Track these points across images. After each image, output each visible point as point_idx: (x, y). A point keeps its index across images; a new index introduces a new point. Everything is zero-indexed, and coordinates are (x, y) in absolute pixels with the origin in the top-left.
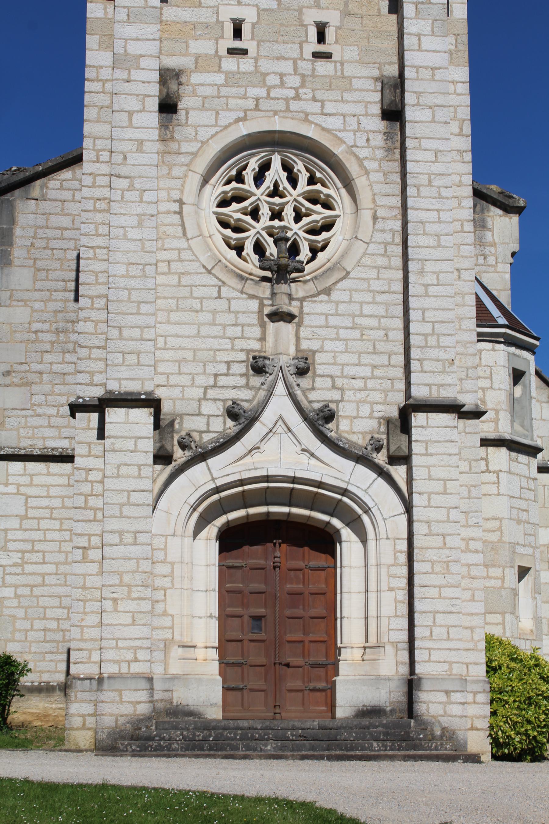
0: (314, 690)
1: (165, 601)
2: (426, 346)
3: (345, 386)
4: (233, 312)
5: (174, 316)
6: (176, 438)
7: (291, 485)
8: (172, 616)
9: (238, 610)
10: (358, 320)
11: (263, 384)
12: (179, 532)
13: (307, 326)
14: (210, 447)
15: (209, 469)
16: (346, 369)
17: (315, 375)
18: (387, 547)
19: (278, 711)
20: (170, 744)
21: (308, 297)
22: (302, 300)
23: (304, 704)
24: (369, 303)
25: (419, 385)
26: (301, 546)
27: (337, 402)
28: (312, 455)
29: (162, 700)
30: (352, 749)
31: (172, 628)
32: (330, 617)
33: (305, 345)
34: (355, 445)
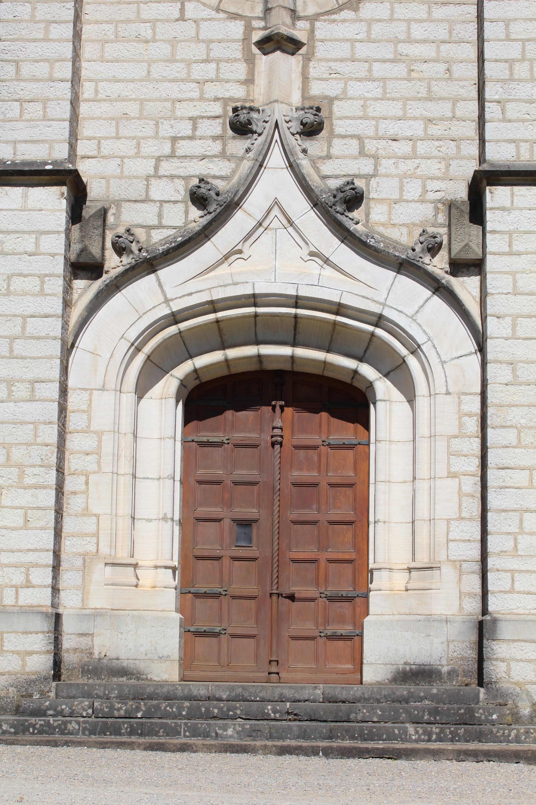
0: (333, 637)
1: (86, 492)
2: (511, 79)
3: (381, 152)
4: (203, 41)
5: (110, 50)
6: (109, 237)
7: (292, 311)
8: (98, 516)
9: (215, 511)
10: (403, 48)
11: (248, 150)
12: (112, 383)
13: (320, 60)
14: (161, 249)
15: (160, 285)
16: (383, 125)
17: (332, 135)
18: (446, 407)
19: (274, 669)
20: (65, 723)
21: (322, 14)
22: (313, 19)
23: (317, 659)
24: (421, 21)
25: (498, 141)
26: (317, 413)
27: (368, 177)
28: (327, 261)
29: (75, 650)
30: (371, 737)
31: (97, 535)
32: (358, 523)
33: (317, 89)
34: (396, 244)
